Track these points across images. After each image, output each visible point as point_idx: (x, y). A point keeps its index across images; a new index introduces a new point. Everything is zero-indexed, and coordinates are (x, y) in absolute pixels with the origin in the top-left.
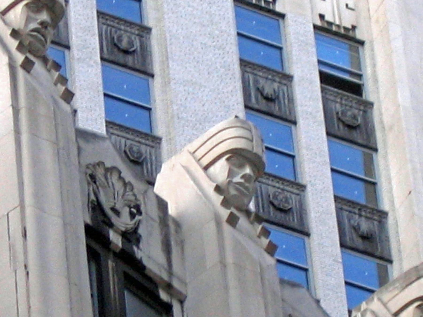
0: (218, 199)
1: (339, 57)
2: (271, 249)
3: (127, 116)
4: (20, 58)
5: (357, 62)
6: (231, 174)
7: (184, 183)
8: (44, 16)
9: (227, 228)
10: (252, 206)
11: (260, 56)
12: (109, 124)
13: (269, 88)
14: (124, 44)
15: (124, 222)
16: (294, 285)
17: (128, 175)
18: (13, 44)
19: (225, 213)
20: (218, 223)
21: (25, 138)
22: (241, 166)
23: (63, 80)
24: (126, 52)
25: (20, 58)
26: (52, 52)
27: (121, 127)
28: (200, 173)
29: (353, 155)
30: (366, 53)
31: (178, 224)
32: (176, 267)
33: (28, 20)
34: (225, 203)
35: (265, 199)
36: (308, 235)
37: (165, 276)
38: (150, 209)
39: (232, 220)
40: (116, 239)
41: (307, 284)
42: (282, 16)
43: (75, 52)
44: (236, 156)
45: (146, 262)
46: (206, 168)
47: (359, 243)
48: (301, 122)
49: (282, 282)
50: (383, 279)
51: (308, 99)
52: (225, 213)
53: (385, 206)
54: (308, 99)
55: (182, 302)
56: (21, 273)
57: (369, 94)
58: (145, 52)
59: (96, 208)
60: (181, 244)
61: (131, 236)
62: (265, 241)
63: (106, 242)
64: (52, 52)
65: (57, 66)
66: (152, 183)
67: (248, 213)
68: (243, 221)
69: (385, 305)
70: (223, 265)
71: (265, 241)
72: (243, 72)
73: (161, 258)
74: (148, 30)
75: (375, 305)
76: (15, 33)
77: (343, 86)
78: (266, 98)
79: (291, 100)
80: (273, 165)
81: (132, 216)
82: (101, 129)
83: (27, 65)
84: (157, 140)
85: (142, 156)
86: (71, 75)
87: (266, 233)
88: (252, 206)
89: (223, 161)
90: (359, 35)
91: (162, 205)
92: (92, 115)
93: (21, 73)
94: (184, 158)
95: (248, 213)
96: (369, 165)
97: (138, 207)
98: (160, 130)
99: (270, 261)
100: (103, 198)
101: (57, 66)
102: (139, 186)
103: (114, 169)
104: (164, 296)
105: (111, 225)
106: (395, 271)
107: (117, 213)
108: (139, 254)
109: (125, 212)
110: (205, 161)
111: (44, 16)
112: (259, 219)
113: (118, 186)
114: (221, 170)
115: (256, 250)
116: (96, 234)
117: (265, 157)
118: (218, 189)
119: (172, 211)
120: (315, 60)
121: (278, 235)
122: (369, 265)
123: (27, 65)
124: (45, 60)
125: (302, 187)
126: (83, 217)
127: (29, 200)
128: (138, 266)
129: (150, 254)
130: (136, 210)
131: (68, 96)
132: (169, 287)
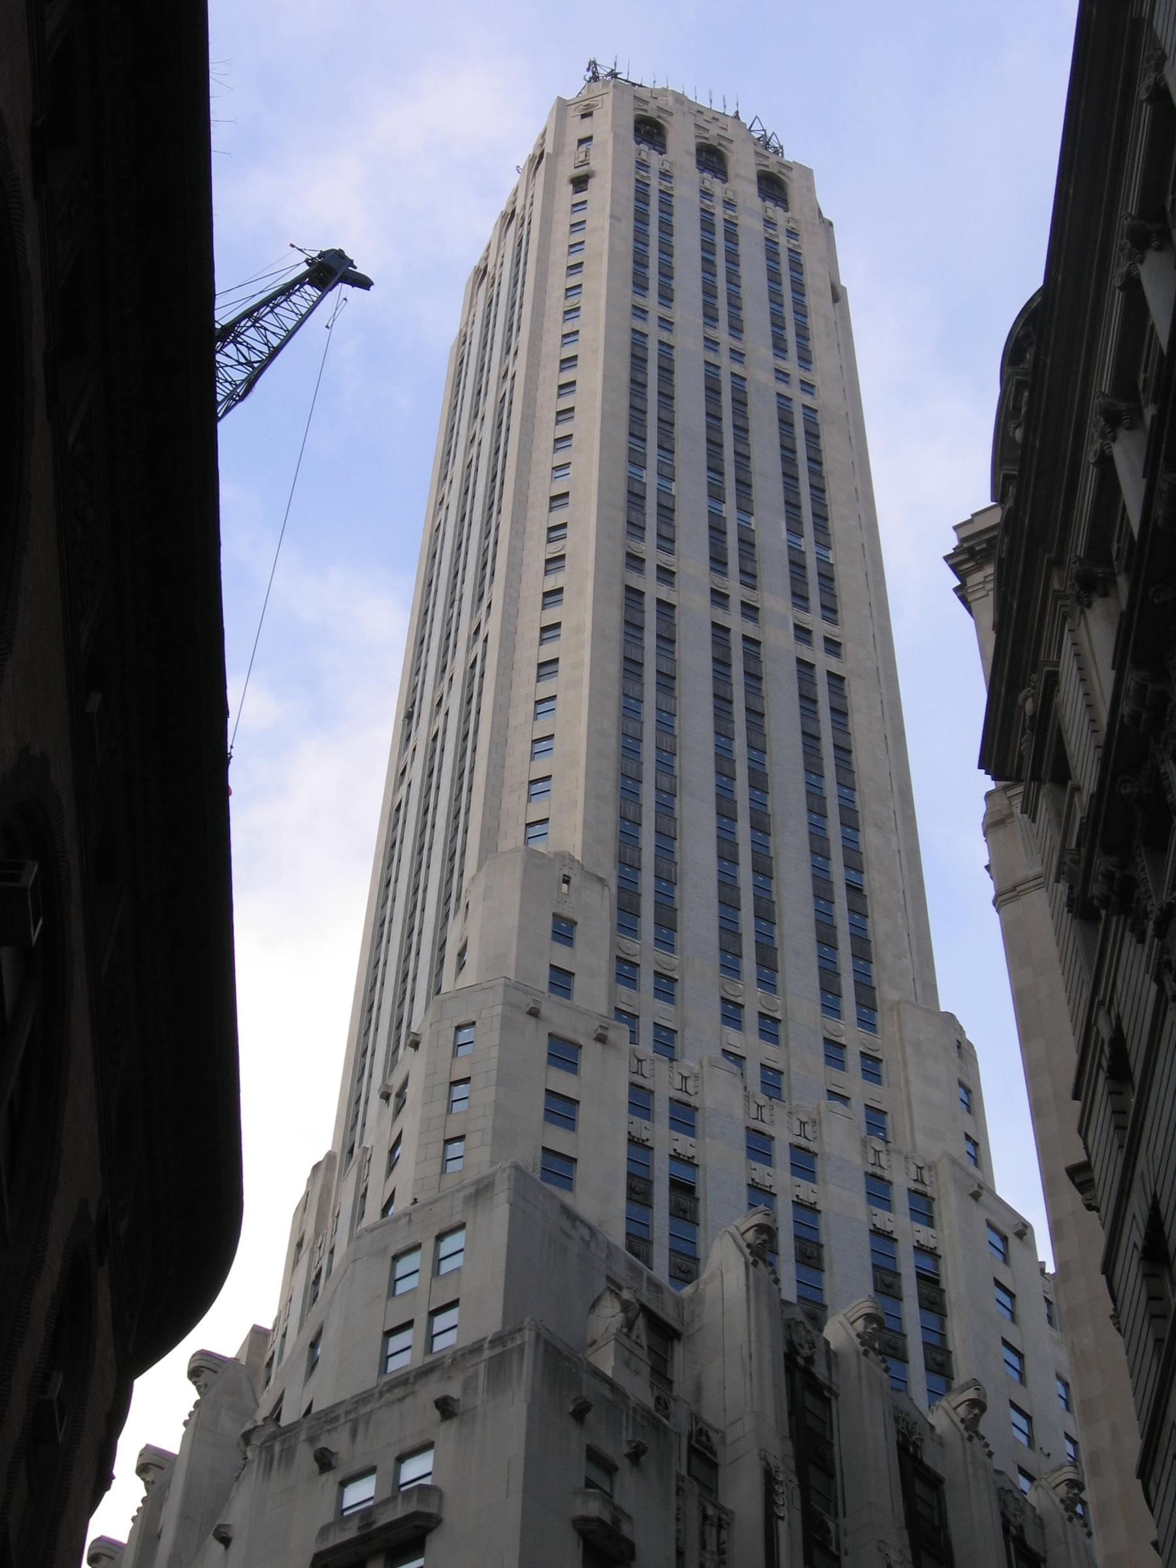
0: (858, 1341)
1: (927, 1263)
2: (887, 1370)
3: (809, 1293)
4: (751, 1259)
5: (937, 1267)
6: (865, 1327)
7: (839, 1332)
8: (765, 1237)
9: (863, 1357)
10: (877, 1345)
11: (884, 1262)
12: (799, 1297)
13: (888, 1280)
14: (808, 1253)
15: (806, 1351)
16: (899, 1390)
17: (809, 1326)
18: (747, 1251)
19: (862, 1349)
20: (858, 1355)
21: (752, 1304)
22: (871, 1323)
23: (774, 1272)
24: (809, 1257)
25: (751, 1259)
26: (768, 1257)
27: (804, 1299)
28: (951, 1412)
29: (933, 1319)
30: (941, 1262)
31: (835, 1354)
32: (834, 1378)
33: (756, 1238)
34: (862, 1344)
35: (883, 1340)
36: (907, 1362)
37: (827, 1382)
38: (820, 1345)
39: (866, 1353)
40: (800, 1361)
41: (906, 1391)
42: (896, 1240)
43: (782, 1257)
44: (869, 1318)
45: (818, 1375)
46: (955, 1409)
47: (935, 1368)
48: (905, 1299)
49: (893, 1388)
50: (949, 1389)
51: (909, 1287)
52: (862, 1349)
53: (951, 1348)
54: (909, 1287)
55: (836, 1398)
56: (748, 1377)
57: (944, 1285)
58: (819, 1258)
59: (790, 1343)
60: (837, 1366)
61: (810, 1360)
62: (883, 1365)
63: (795, 1363)
64: (768, 1257)
65: (771, 1264)
66: (821, 1331)
67: (874, 1349)
68: (872, 1354)
69: (949, 1403)
70: (860, 1377)
71: (883, 1365)
72: (874, 1271)
73: (826, 1373)
74: (822, 1246)
75: (944, 1403)
76: (749, 1246)
77: (930, 1282)
78: (886, 1284)
79: (900, 1287)
80: (889, 1323)
81: (810, 1349)
82: (794, 1300)
83: (755, 1263)
84: (825, 1307)
85: (816, 1314)
86: (1081, 1517)
87: (884, 1361)
88: (877, 1345)
89: (752, 1231)
90: (939, 1252)
91: (827, 1343)
92: (789, 1291)
93: (751, 1268)
94: (840, 1317)
95: (874, 1349)
96: (942, 1326)
97: (813, 1344)
98: (827, 1302)
99: (886, 1376)
100: (795, 1338)
101: (771, 1264)
102: (815, 1333)
103: (801, 1322)
104: (826, 1394)
105: (798, 1353)
106: (955, 1384)
107: (802, 1346)
108: (814, 1370)
109: (807, 1346)
110: (852, 1320)
111: (765, 1237)
112: (880, 1353)
113: (803, 1332)
114: (860, 1325)
115: (878, 1370)
116: (790, 1359)
117: (885, 1318)
118: (858, 1335)
119: (832, 1347)
120: (913, 1265)
121: (890, 1362)
122: (939, 1381)
123: (755, 1263)
124: (764, 1261)
125: (905, 1336)
126: (782, 1348)
127: (753, 1338)
128: (813, 1377)
129: (820, 1370)
130: (812, 1345)
131: (777, 1281)
132: (830, 1389)
